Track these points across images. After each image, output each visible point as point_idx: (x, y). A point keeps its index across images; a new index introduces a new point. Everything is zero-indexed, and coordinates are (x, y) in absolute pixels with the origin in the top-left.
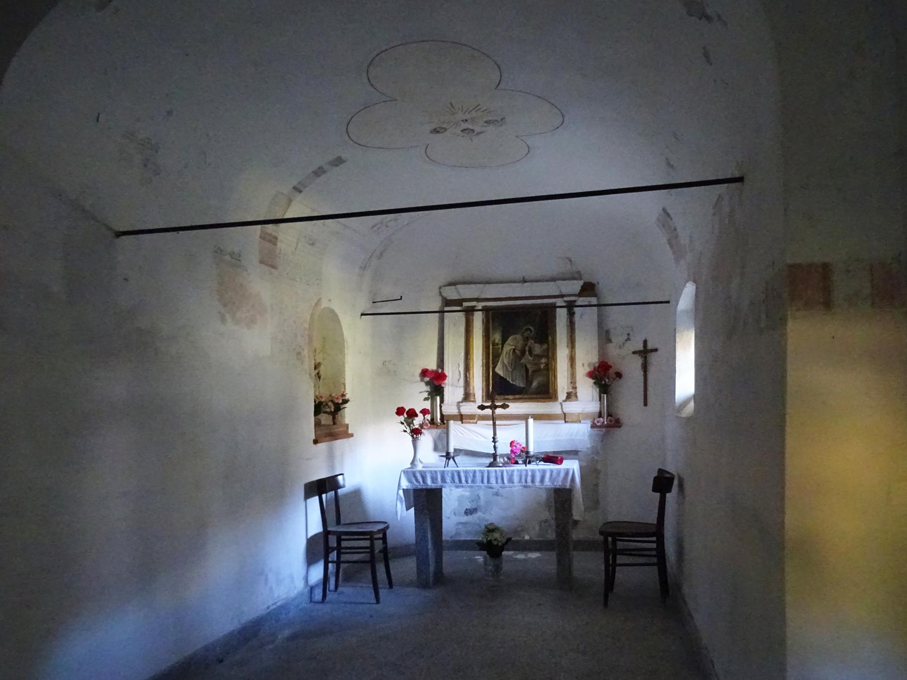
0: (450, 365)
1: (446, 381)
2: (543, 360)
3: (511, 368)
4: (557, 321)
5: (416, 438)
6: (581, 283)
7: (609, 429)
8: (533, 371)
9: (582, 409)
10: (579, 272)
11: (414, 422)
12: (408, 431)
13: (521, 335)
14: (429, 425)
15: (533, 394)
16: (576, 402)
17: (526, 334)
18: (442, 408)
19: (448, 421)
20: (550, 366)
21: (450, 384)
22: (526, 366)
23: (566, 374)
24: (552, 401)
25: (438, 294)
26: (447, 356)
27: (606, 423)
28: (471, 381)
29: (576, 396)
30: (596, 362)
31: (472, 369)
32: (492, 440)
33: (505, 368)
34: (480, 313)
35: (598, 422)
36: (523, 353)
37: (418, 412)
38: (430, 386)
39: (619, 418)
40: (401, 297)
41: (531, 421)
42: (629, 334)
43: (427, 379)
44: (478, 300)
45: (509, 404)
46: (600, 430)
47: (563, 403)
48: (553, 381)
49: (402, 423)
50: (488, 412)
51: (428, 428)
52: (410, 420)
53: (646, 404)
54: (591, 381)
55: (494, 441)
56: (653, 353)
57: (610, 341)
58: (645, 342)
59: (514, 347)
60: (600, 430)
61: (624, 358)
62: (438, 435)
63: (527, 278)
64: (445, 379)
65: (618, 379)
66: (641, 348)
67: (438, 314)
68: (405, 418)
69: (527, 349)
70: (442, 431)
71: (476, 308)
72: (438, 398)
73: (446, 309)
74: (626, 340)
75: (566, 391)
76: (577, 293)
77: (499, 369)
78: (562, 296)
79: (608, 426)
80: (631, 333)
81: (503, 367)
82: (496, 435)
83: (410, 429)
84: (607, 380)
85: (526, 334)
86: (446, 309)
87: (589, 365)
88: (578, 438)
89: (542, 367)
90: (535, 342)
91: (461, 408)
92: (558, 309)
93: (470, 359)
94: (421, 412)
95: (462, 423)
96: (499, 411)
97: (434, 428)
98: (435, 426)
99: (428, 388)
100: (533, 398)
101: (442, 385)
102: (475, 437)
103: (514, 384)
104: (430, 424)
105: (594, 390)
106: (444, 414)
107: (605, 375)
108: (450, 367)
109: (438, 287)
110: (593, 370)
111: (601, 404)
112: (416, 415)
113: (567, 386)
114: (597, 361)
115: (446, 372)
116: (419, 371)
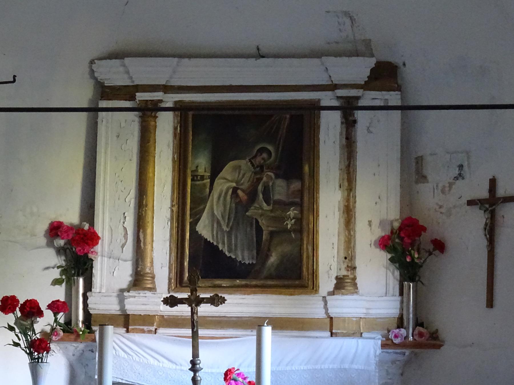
0: (107, 215)
1: (98, 248)
2: (292, 212)
3: (227, 226)
4: (322, 136)
5: (38, 358)
6: (371, 62)
7: (417, 350)
8: (272, 234)
9: (365, 311)
10: (367, 43)
11: (35, 326)
12: (23, 343)
13: (250, 160)
14: (61, 333)
15: (270, 277)
16: (355, 297)
17: (259, 160)
18: (89, 301)
19: (102, 326)
20: (304, 223)
21: (106, 254)
22: (257, 222)
23: (335, 240)
24: (306, 293)
25: (87, 76)
26: (102, 168)
27: (411, 338)
28: (149, 247)
29: (355, 285)
30: (396, 220)
31: (149, 225)
32: (190, 366)
33: (215, 226)
34: (170, 114)
35: (396, 336)
36: (252, 196)
37: (43, 306)
38: (66, 256)
39: (437, 331)
40: (14, 77)
41: (267, 330)
42: (461, 167)
43: (60, 242)
44: (167, 89)
45: (226, 296)
46: (400, 353)
47: (328, 298)
48: (311, 254)
49: (11, 329)
50: (184, 310)
51: (59, 340)
52: (27, 323)
53: (490, 304)
54: (384, 256)
55: (194, 367)
56: (507, 204)
57: (422, 178)
58: (493, 182)
59: (234, 185)
60: (400, 353)
61: (449, 213)
62: (77, 354)
63: (264, 50)
64: (97, 243)
65: (437, 252)
66: (484, 194)
67: (85, 114)
68: (17, 319)
69: (260, 187)
70: (87, 346)
71: (163, 105)
72: (81, 281)
73: (103, 104)
74: (456, 178)
75: (334, 274)
76: (363, 83)
77: (205, 226)
78: (333, 87)
79: (416, 345)
80: (465, 164)
81: (213, 221)
82: (198, 356)
83: (27, 340)
84: (416, 256)
85: (259, 160)
86: (103, 104)
87: (382, 223)
88: (355, 366)
89: (289, 226)
90: (277, 176)
91: (126, 301)
92: (323, 113)
93: (146, 206)
94: (50, 307)
95: (128, 331)
96: (204, 310)
97: (70, 340)
98: (73, 337)
99: (61, 261)
100: (270, 287)
101: (90, 256)
102: (151, 360)
103: (233, 257)
104: (64, 331)
105: (390, 274)
106: (91, 312)
107: (412, 245)
108: (107, 220)
109: (88, 61)
110: (388, 233)
111: (402, 302)
112: (40, 313)
113: (338, 262)
114: (398, 217)
115: (99, 229)
116: (44, 226)
